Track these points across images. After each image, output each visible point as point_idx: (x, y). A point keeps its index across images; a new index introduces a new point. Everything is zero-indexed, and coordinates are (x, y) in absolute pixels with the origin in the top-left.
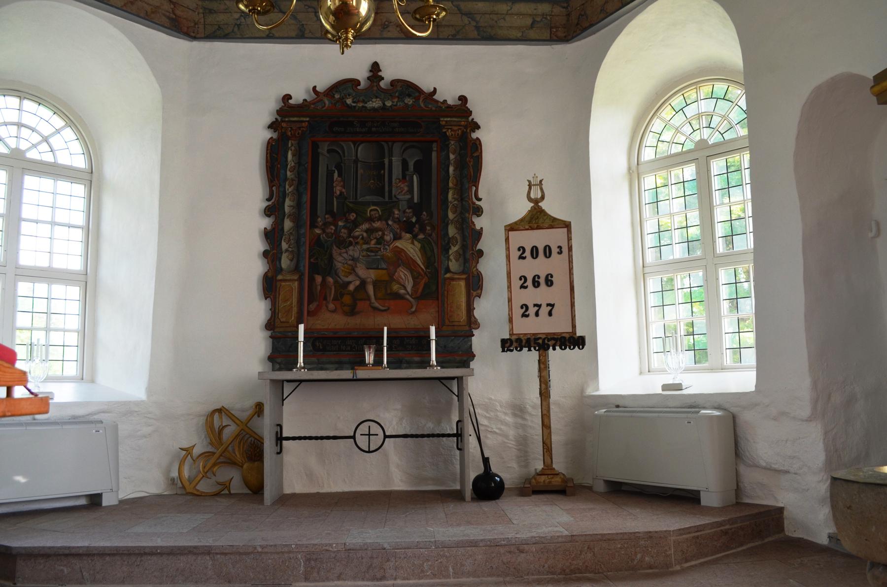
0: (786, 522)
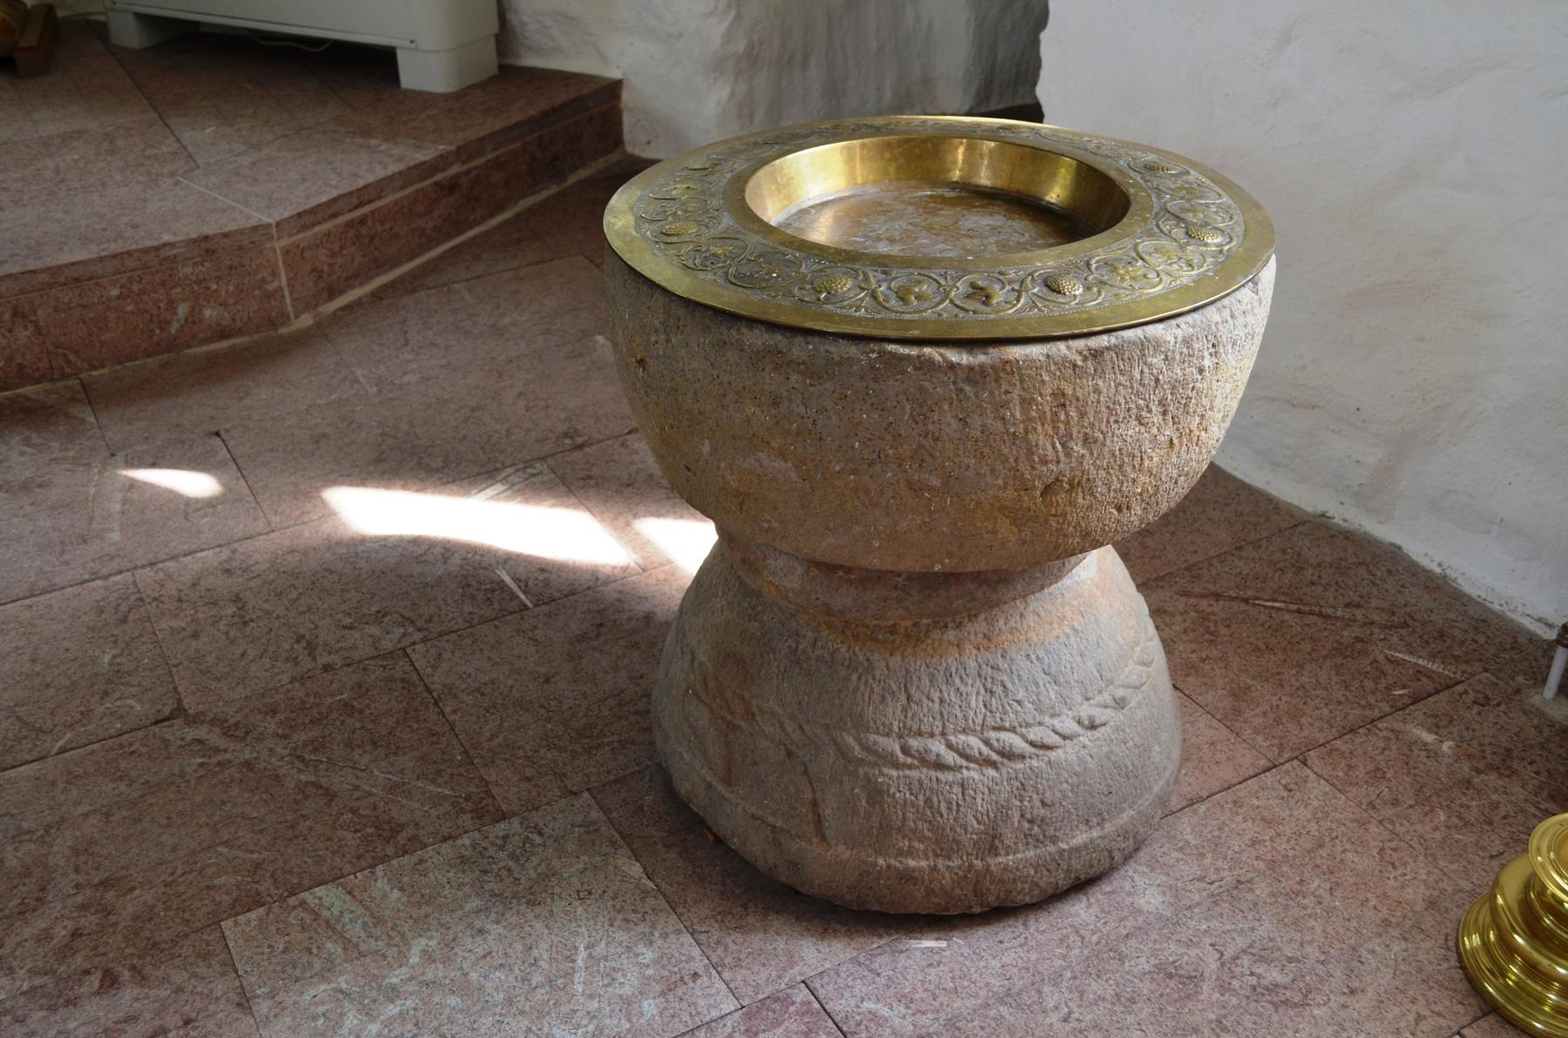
0: (627, 120)
